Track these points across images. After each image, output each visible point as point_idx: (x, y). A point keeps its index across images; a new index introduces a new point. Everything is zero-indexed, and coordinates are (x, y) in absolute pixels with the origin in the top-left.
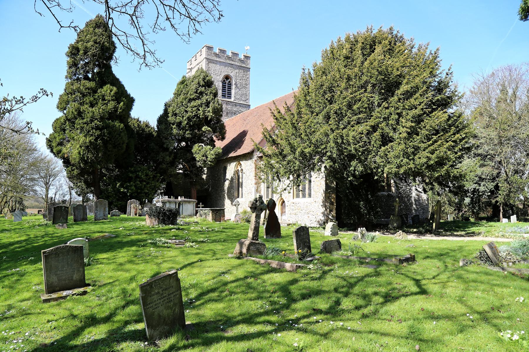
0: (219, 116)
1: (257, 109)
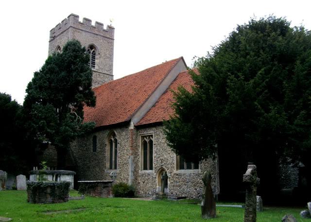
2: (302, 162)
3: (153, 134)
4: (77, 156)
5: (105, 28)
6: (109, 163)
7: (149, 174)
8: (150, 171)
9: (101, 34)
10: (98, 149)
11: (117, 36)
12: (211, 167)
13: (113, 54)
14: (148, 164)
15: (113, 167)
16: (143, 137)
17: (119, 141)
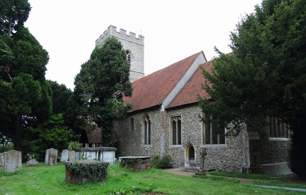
3: (181, 115)
4: (119, 135)
5: (137, 37)
6: (144, 139)
7: (177, 148)
8: (179, 145)
11: (146, 42)
12: (237, 142)
14: (177, 139)
15: (148, 142)
16: (172, 118)
17: (151, 121)
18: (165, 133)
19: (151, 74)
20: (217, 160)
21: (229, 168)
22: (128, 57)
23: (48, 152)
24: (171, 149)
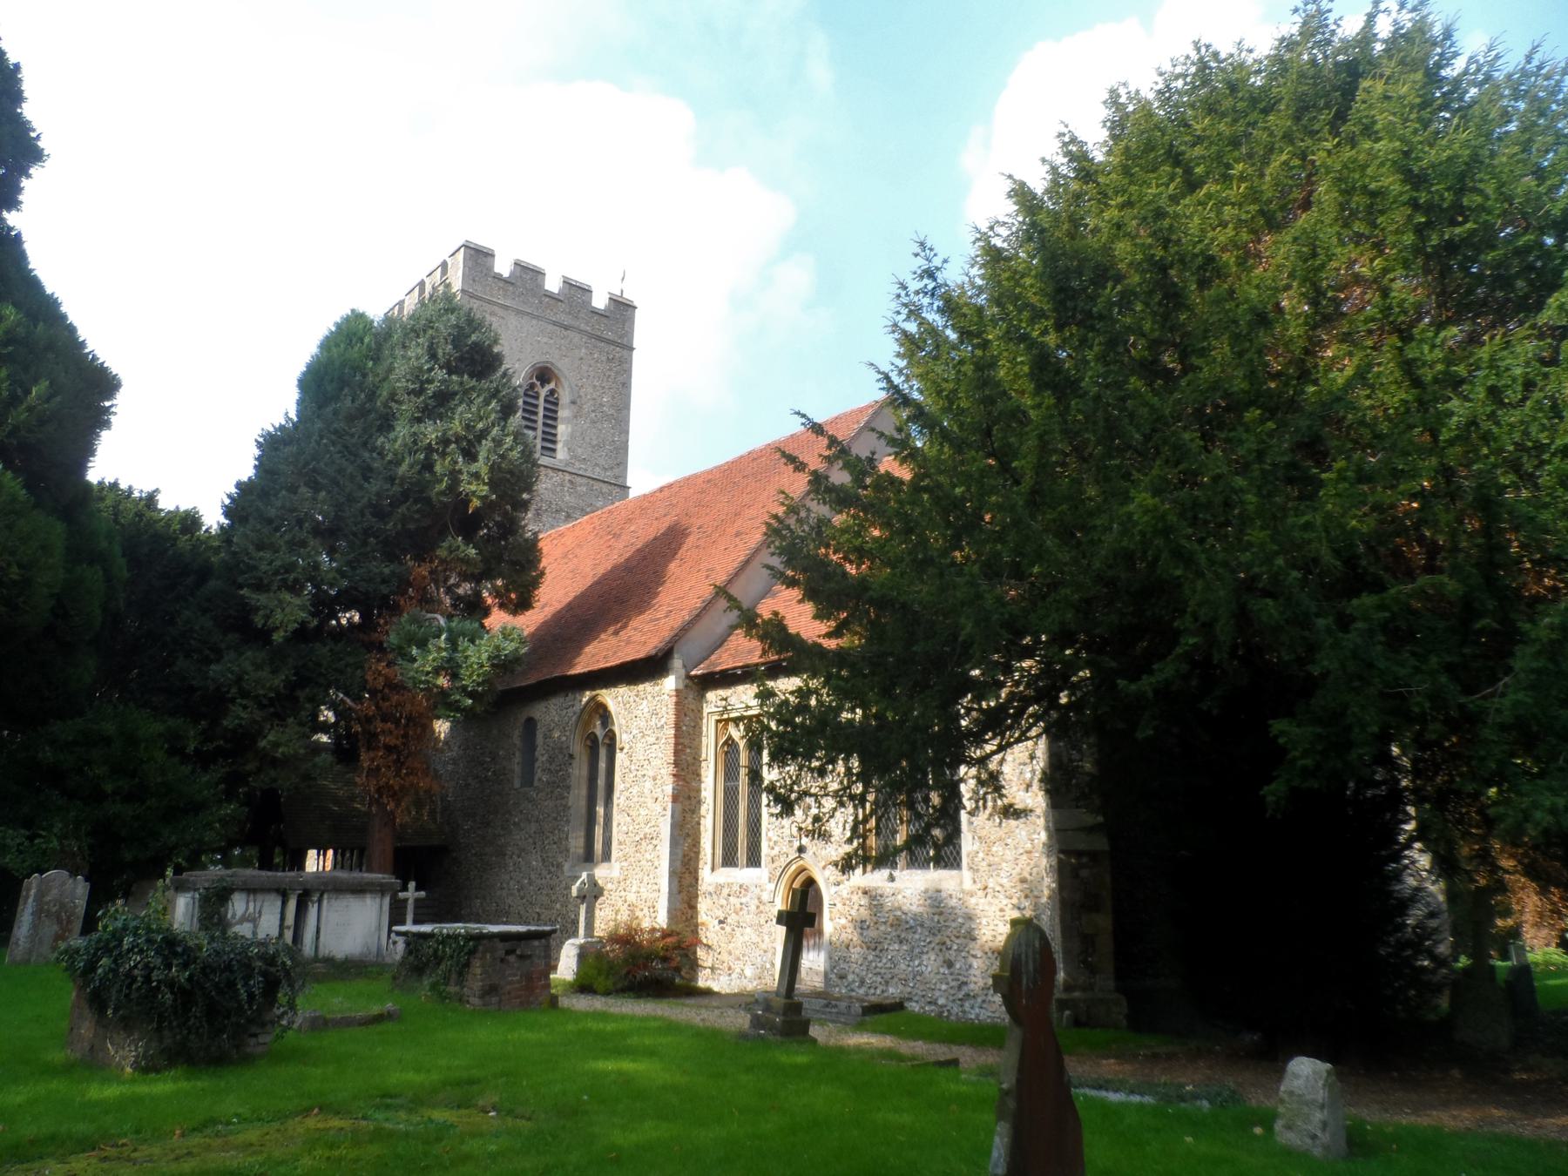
0: (515, 508)
1: (666, 493)
2: (272, 859)
9: (583, 326)
10: (539, 774)
13: (627, 406)
18: (687, 803)
19: (653, 494)
20: (925, 957)
21: (979, 1000)
22: (546, 401)
23: (33, 892)
24: (711, 889)
